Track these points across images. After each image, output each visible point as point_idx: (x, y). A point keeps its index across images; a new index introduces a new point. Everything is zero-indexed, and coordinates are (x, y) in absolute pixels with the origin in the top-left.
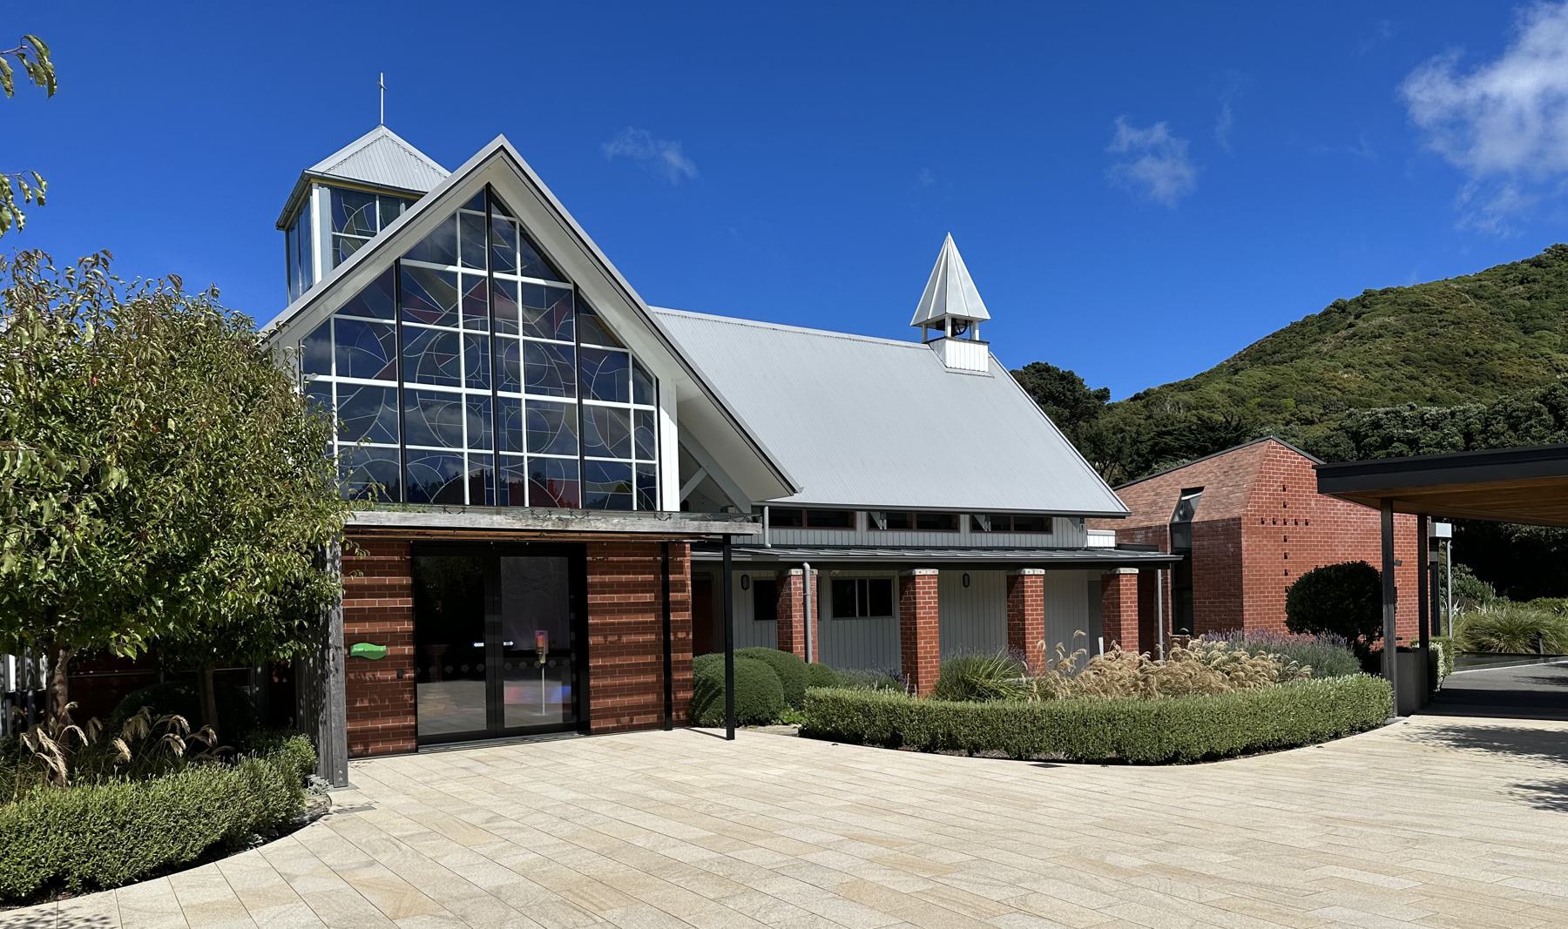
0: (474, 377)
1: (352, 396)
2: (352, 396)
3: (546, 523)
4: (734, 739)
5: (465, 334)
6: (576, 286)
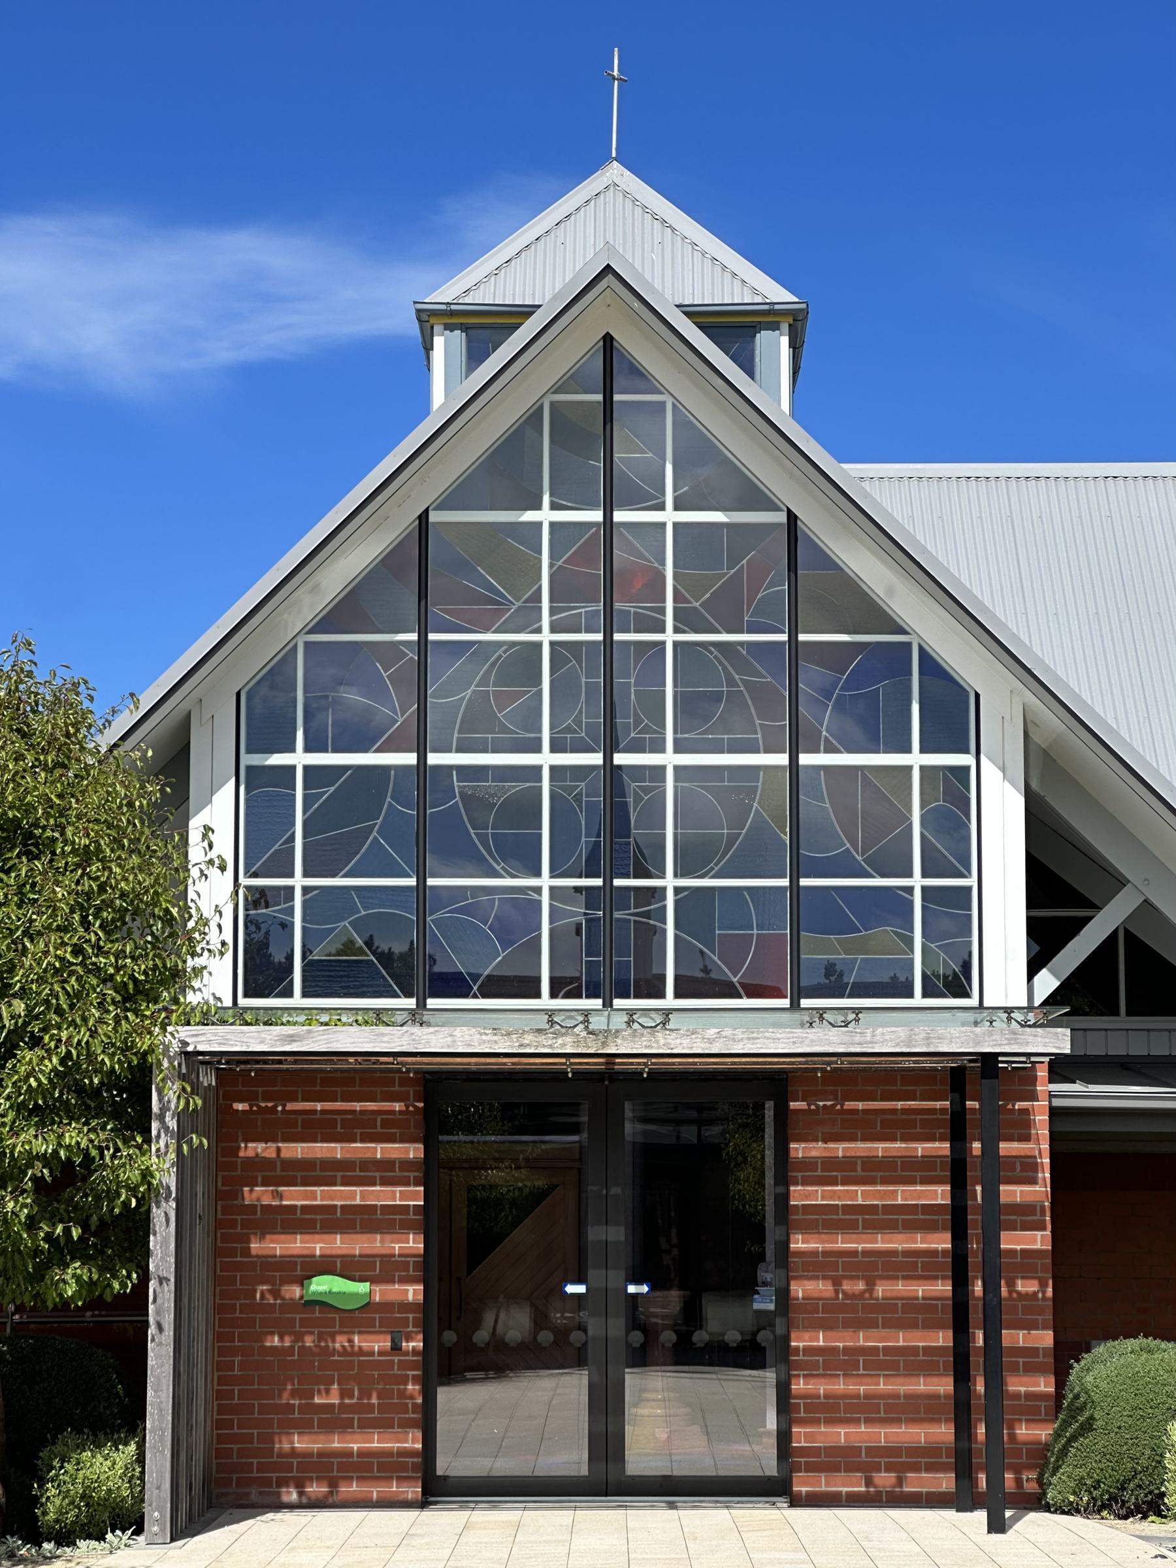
0: (568, 729)
1: (332, 789)
2: (332, 789)
3: (560, 1041)
4: (989, 1532)
5: (552, 644)
6: (792, 518)
